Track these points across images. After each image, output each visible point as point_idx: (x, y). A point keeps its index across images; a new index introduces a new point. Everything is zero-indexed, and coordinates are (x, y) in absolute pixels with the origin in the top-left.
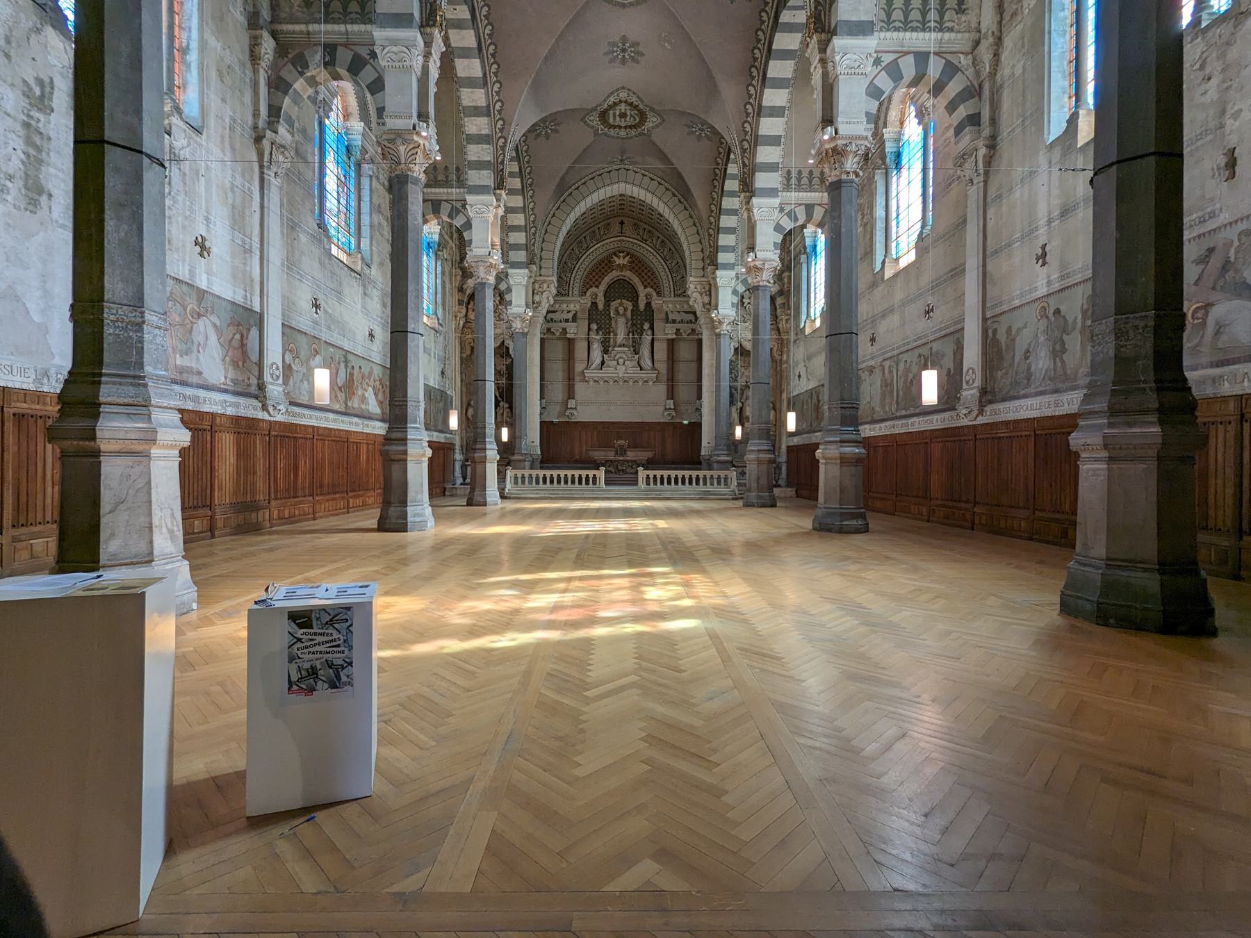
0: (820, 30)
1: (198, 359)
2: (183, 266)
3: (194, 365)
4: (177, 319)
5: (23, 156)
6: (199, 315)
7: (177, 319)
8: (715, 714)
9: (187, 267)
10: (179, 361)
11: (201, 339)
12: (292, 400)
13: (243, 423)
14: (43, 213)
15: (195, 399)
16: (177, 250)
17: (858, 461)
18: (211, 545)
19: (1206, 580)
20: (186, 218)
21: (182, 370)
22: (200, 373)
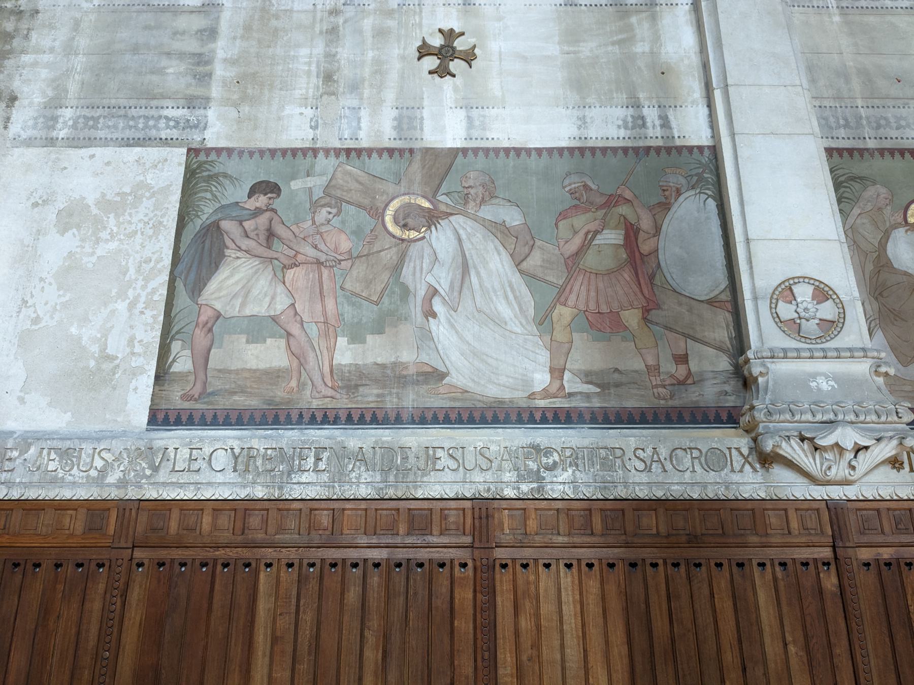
1: (426, 336)
3: (407, 356)
6: (432, 218)
7: (345, 244)
11: (443, 279)
16: (355, 87)
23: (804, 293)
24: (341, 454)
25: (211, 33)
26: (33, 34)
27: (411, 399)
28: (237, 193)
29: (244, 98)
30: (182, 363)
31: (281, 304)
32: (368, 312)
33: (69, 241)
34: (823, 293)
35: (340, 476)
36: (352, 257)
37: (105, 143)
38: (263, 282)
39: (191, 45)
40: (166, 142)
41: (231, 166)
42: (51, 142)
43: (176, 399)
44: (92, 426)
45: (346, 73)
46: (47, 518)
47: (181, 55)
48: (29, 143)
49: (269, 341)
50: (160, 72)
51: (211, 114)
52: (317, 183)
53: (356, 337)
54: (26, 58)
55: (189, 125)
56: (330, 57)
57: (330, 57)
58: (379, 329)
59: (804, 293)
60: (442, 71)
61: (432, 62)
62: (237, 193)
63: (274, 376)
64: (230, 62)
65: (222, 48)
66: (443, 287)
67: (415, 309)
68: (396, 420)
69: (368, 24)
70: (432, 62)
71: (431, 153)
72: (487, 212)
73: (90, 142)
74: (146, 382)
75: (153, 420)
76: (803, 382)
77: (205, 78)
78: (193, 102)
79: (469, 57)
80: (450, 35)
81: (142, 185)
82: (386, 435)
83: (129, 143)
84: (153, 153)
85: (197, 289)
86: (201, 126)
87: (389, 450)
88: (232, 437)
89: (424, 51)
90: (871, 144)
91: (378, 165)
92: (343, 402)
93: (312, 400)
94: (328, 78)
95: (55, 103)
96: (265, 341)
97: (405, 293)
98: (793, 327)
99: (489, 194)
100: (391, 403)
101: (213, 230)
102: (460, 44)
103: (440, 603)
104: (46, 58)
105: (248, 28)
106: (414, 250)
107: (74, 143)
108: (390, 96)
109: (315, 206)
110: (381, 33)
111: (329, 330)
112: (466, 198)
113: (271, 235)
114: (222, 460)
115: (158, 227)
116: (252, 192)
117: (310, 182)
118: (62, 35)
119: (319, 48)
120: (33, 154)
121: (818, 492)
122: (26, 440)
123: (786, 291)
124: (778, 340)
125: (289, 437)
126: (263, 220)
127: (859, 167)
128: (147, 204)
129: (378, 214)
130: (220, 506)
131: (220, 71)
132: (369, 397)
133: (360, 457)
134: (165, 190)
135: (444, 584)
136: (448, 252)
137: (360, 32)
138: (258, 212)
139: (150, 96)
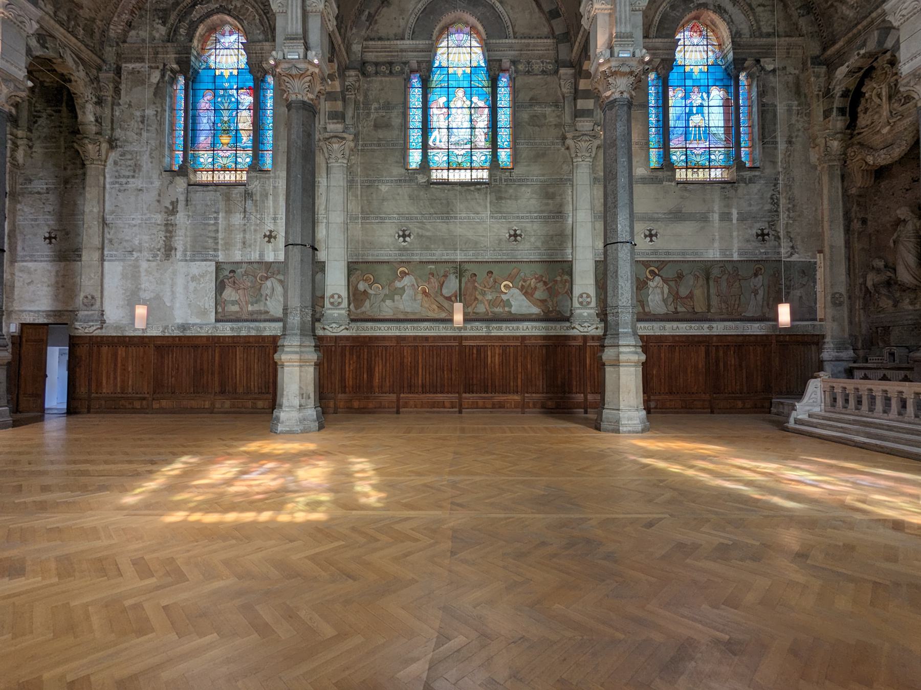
0: (837, 296)
1: (265, 304)
2: (255, 252)
3: (262, 308)
4: (249, 284)
5: (164, 239)
6: (267, 278)
7: (249, 284)
8: (316, 250)
9: (258, 253)
10: (250, 308)
11: (269, 292)
12: (449, 325)
13: (216, 340)
14: (172, 259)
15: (257, 329)
16: (250, 246)
17: (547, 347)
18: (368, 398)
19: (23, 325)
20: (257, 225)
21: (252, 313)
22: (267, 312)
23: (336, 296)
24: (249, 328)
25: (217, 231)
26: (97, 243)
27: (263, 317)
28: (227, 273)
29: (226, 249)
30: (220, 310)
31: (237, 298)
32: (254, 299)
33: (194, 284)
34: (339, 297)
35: (249, 331)
36: (251, 287)
37: (198, 261)
38: (233, 293)
39: (213, 234)
40: (211, 260)
41: (225, 266)
42: (186, 260)
43: (219, 317)
44: (205, 322)
45: (248, 242)
46: (200, 339)
47: (211, 237)
48: (182, 261)
49: (841, 544)
50: (207, 242)
51: (219, 253)
52: (243, 270)
53: (252, 305)
54: (177, 238)
55: (215, 256)
56: (244, 237)
57: (244, 237)
58: (256, 303)
59: (336, 296)
60: (269, 242)
61: (267, 239)
62: (227, 273)
63: (237, 312)
64: (222, 239)
65: (220, 235)
66: (269, 294)
67: (263, 298)
68: (260, 321)
69: (252, 228)
70: (267, 239)
71: (266, 262)
72: (278, 277)
73: (195, 260)
74: (214, 314)
75: (217, 321)
76: (331, 314)
77: (217, 243)
78: (216, 250)
79: (275, 238)
80: (271, 232)
81: (206, 271)
82: (257, 324)
83: (203, 261)
84: (208, 263)
85: (221, 294)
86: (217, 256)
87: (258, 327)
88: (230, 324)
89: (265, 236)
90: (360, 260)
91: (255, 266)
92: (250, 318)
93: (244, 317)
94: (244, 243)
95: (185, 250)
96: (844, 545)
97: (261, 295)
98: (332, 304)
99: (279, 273)
100: (259, 318)
101: (222, 282)
102: (273, 234)
103: (267, 353)
104: (181, 238)
105: (225, 229)
106: (263, 286)
107: (191, 261)
108: (258, 248)
109: (243, 275)
110: (255, 231)
111: (247, 304)
112: (274, 274)
113: (234, 282)
114: (228, 329)
115: (212, 281)
116: (230, 272)
117: (242, 270)
118: (183, 231)
119: (242, 235)
120: (183, 263)
121: (332, 334)
122: (194, 325)
123: (332, 296)
124: (330, 306)
125: (240, 324)
126: (232, 279)
127: (356, 266)
128: (209, 275)
129: (256, 278)
130: (229, 337)
131: (220, 242)
132: (255, 316)
133: (252, 328)
134: (212, 272)
135: (268, 350)
136: (22, 233)
137: (251, 230)
138: (231, 277)
139: (206, 248)
